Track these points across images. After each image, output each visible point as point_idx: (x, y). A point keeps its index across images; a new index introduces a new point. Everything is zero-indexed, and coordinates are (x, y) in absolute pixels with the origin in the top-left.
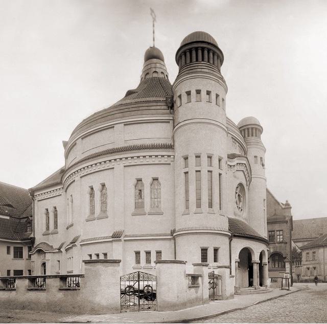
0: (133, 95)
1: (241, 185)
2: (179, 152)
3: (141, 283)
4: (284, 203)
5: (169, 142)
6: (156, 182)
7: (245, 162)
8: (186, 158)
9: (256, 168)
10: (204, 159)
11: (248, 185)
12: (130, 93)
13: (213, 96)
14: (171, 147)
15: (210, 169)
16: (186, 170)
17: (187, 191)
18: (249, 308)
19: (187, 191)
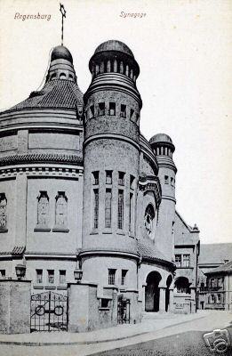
0: (38, 97)
1: (150, 206)
2: (90, 167)
3: (52, 303)
4: (193, 226)
5: (29, 180)
6: (61, 199)
7: (155, 182)
8: (96, 174)
9: (166, 190)
10: (115, 176)
11: (157, 207)
12: (33, 95)
13: (118, 109)
14: (81, 163)
15: (121, 188)
16: (96, 187)
17: (96, 209)
18: (74, 148)
19: (96, 209)
